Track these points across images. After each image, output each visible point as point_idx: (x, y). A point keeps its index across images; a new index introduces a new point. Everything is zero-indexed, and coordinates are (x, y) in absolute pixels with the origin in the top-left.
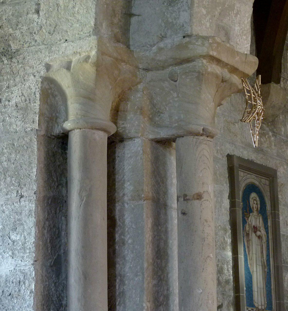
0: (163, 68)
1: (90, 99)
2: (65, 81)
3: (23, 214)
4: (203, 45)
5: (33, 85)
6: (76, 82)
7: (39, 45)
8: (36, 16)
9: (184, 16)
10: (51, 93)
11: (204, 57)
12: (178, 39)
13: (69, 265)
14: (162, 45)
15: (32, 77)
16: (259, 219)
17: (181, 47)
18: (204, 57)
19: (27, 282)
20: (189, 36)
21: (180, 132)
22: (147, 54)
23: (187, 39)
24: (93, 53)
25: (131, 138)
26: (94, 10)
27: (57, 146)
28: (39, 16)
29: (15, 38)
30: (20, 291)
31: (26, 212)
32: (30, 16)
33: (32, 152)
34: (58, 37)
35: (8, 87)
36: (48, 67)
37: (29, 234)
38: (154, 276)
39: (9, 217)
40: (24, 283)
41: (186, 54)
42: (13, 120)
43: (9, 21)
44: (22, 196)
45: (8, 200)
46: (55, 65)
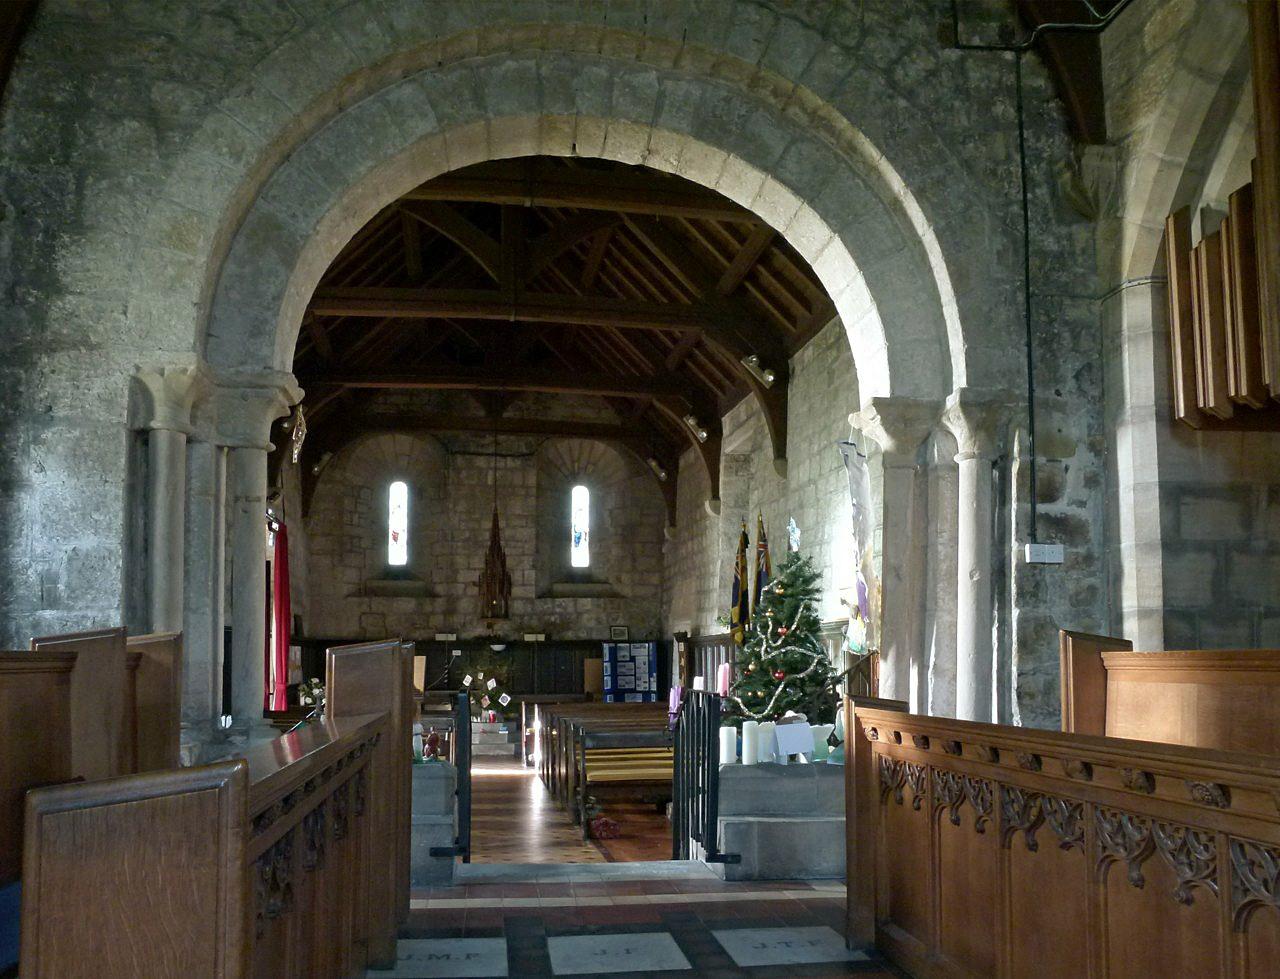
0: (237, 387)
1: (178, 405)
2: (155, 386)
3: (108, 498)
4: (282, 378)
5: (120, 382)
6: (168, 388)
7: (127, 345)
8: (122, 317)
9: (265, 351)
10: (140, 392)
11: (278, 387)
12: (258, 368)
13: (971, 474)
14: (241, 369)
15: (119, 374)
16: (857, 483)
17: (260, 375)
18: (278, 387)
19: (113, 559)
20: (270, 368)
21: (241, 443)
22: (224, 372)
23: (269, 371)
24: (192, 368)
25: (200, 442)
26: (193, 329)
27: (142, 437)
28: (127, 317)
29: (96, 332)
30: (104, 565)
31: (111, 496)
32: (115, 314)
33: (120, 442)
34: (151, 343)
35: (88, 377)
36: (138, 368)
37: (116, 516)
38: (810, 481)
39: (90, 498)
40: (110, 559)
41: (262, 382)
42: (94, 409)
43: (1028, 580)
44: (106, 481)
45: (89, 482)
46: (146, 368)
